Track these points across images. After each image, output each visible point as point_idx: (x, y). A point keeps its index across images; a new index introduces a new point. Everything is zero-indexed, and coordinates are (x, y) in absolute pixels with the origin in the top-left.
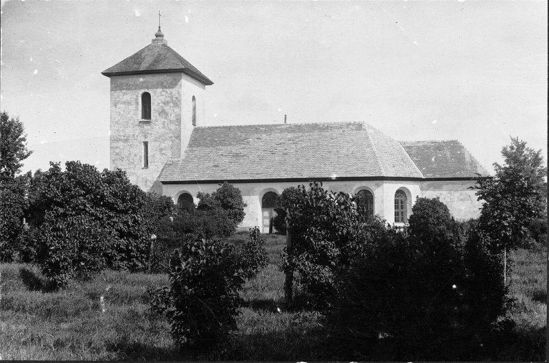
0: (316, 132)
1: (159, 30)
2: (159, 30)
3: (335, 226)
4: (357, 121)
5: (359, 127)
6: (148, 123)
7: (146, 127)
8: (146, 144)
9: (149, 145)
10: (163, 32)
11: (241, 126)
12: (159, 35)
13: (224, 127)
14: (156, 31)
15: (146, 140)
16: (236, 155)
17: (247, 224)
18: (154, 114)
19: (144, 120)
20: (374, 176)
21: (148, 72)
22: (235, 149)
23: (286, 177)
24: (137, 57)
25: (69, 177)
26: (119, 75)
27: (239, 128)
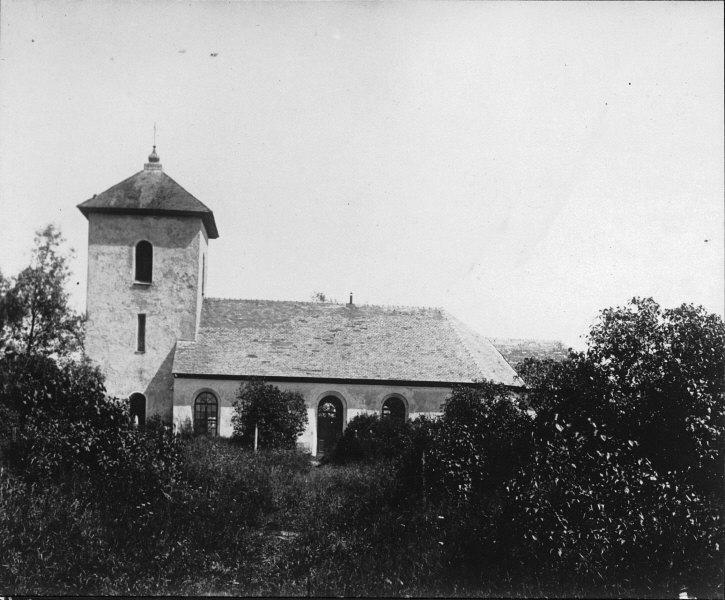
0: (381, 317)
1: (154, 152)
2: (154, 152)
3: (85, 465)
4: (433, 307)
5: (439, 315)
6: (146, 288)
7: (146, 295)
8: (142, 318)
9: (147, 319)
10: (159, 154)
11: (272, 302)
12: (153, 159)
13: (247, 301)
14: (149, 152)
15: (144, 312)
16: (276, 343)
17: (534, 417)
18: (156, 276)
19: (138, 282)
20: (402, 379)
21: (150, 218)
22: (274, 334)
23: (355, 376)
24: (127, 186)
25: (537, 396)
26: (95, 213)
27: (270, 303)
